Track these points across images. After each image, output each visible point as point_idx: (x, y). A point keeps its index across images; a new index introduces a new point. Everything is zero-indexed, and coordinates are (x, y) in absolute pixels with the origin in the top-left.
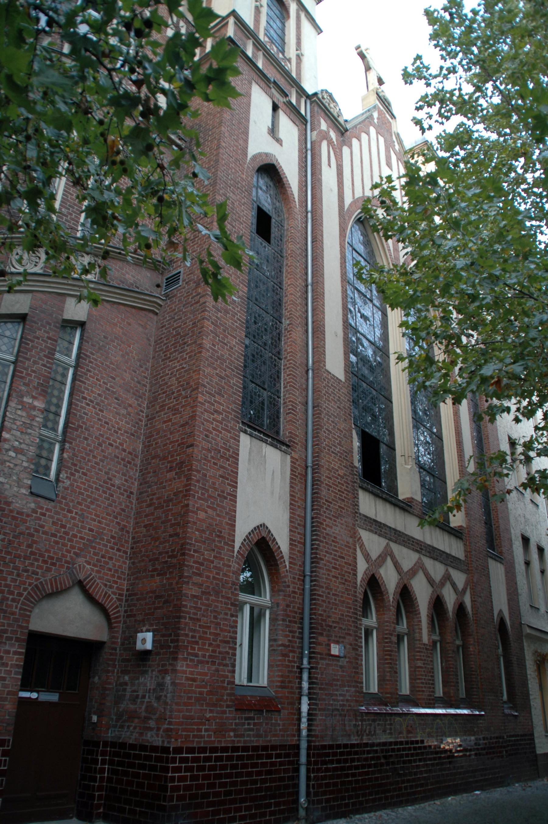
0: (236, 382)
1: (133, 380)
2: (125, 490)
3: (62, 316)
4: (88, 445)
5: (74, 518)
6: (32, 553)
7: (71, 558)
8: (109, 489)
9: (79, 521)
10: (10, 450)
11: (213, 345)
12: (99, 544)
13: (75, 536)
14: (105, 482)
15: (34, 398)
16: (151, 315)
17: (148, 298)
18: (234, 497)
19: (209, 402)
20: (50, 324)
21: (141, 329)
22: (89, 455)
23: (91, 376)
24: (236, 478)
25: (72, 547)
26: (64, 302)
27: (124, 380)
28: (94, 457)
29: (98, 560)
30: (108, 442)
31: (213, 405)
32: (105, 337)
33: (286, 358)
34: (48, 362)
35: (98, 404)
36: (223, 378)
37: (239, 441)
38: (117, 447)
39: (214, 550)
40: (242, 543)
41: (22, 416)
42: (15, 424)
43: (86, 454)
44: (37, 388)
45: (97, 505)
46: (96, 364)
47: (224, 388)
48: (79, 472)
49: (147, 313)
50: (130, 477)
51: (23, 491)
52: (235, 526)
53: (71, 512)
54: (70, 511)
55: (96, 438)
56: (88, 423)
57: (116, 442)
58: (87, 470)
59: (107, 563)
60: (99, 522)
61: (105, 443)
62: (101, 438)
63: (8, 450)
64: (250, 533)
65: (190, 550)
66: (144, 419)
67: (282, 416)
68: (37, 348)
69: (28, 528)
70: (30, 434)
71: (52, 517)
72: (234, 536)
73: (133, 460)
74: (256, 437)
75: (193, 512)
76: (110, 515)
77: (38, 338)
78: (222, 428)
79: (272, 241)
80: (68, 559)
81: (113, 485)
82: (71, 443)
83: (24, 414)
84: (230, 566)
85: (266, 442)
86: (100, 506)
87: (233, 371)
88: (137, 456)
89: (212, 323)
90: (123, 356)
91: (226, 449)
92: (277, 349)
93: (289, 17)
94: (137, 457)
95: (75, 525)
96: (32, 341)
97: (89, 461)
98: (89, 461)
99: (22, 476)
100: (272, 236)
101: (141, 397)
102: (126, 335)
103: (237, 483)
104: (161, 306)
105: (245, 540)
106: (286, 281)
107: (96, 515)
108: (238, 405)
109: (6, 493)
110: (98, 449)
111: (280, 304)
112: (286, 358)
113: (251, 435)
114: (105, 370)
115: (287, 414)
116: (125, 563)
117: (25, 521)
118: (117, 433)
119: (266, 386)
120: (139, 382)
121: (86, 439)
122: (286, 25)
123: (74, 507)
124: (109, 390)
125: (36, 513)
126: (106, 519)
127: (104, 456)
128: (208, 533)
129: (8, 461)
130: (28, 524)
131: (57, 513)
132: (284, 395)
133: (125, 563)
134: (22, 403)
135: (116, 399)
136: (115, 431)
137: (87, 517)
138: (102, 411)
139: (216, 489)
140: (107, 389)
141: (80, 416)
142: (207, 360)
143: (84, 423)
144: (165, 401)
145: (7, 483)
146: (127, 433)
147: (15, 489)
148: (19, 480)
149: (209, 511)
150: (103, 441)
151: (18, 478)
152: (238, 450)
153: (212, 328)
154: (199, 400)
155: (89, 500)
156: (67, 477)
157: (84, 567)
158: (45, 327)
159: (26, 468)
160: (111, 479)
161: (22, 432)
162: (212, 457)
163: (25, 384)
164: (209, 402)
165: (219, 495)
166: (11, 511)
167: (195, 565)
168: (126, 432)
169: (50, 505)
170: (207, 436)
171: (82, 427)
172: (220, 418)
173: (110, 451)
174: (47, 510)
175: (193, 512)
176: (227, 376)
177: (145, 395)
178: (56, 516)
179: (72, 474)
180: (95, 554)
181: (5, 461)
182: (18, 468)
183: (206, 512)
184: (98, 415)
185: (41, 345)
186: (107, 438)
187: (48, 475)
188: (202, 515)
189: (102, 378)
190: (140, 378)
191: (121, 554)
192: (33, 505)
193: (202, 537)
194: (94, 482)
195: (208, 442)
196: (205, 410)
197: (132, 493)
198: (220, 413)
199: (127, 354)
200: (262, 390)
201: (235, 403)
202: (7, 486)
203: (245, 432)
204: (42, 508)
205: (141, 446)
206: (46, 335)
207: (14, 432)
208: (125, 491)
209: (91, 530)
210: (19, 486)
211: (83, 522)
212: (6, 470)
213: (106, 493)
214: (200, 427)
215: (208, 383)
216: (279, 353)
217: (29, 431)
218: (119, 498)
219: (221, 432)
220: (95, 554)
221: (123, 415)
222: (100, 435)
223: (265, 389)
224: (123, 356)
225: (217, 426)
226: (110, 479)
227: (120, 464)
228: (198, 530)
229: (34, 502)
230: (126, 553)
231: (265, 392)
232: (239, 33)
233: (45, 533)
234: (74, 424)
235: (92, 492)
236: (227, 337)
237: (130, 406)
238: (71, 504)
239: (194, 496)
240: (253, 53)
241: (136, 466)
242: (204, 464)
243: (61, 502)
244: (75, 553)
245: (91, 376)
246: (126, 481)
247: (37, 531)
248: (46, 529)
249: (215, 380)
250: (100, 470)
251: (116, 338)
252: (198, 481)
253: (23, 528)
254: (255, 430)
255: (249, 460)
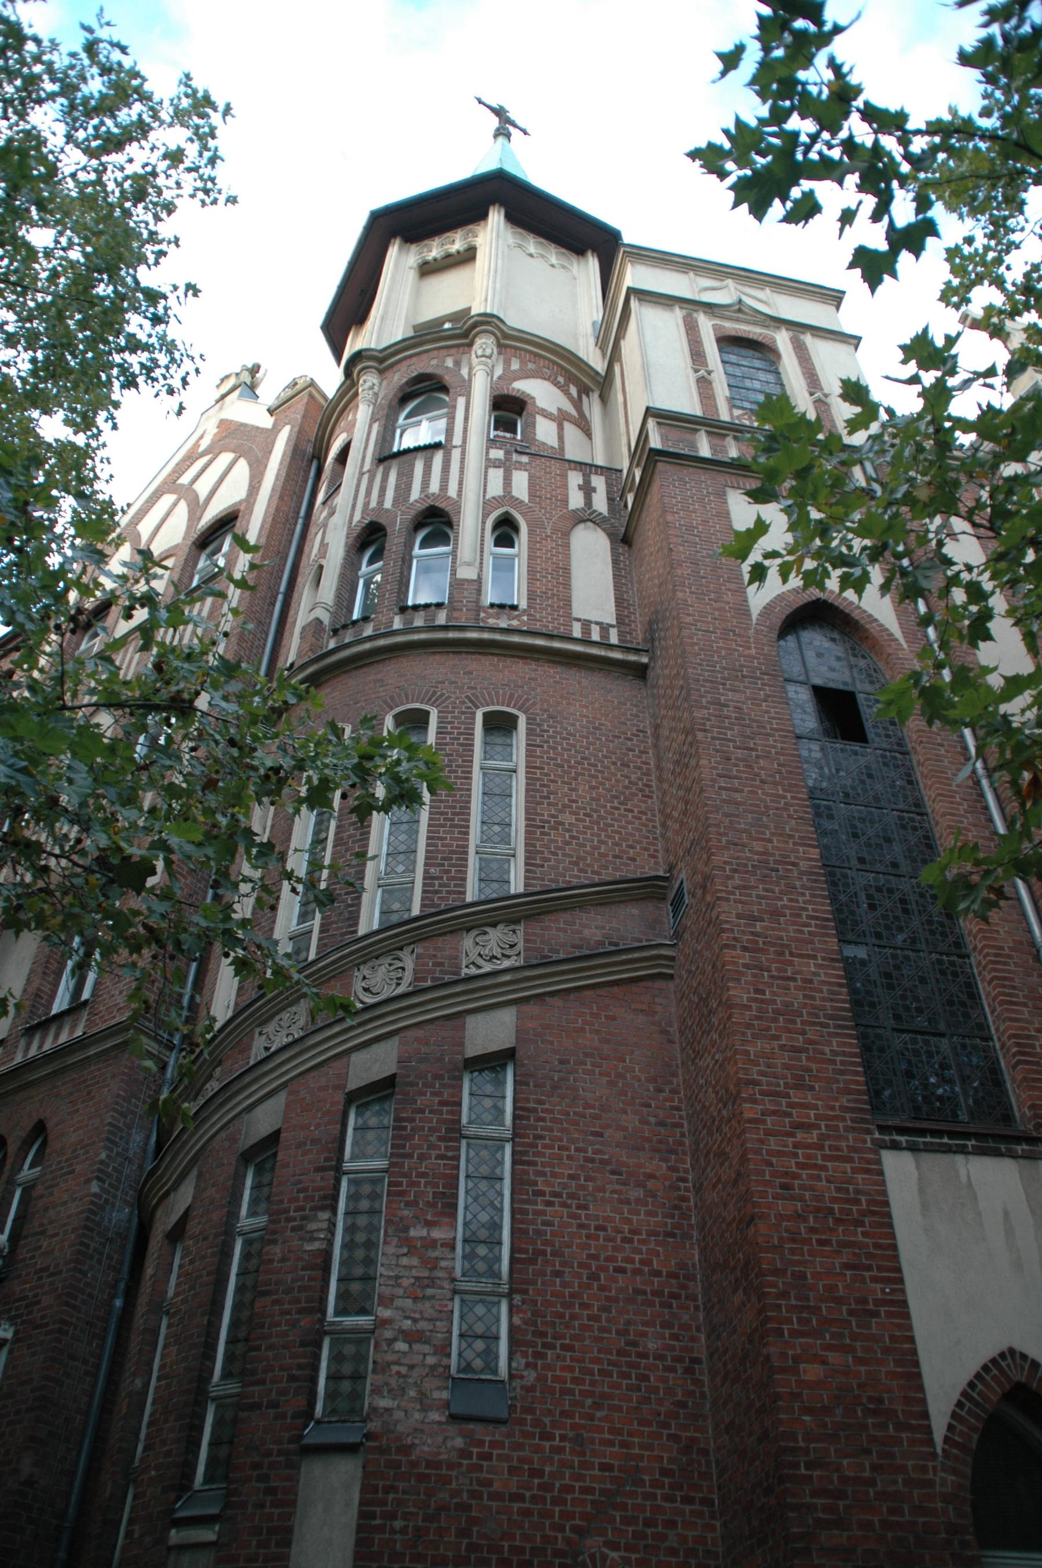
0: (841, 1046)
1: (648, 1123)
2: (676, 1359)
3: (462, 1053)
4: (565, 1285)
5: (560, 1450)
6: (472, 1548)
7: (568, 1541)
8: (636, 1366)
9: (573, 1451)
10: (395, 1339)
11: (757, 991)
12: (633, 1494)
13: (570, 1489)
14: (620, 1353)
15: (429, 1224)
16: (660, 984)
17: (636, 955)
18: (900, 1308)
19: (774, 1113)
20: (440, 1077)
21: (641, 1018)
22: (571, 1306)
23: (545, 1146)
24: (896, 1258)
25: (566, 1515)
26: (463, 1028)
27: (625, 1129)
28: (584, 1306)
29: (638, 1536)
30: (611, 1266)
31: (790, 1115)
32: (562, 1062)
33: (975, 949)
34: (447, 1148)
35: (571, 1196)
36: (800, 1050)
37: (881, 1173)
38: (636, 1272)
39: (868, 1452)
40: (954, 1415)
41: (411, 1267)
42: (399, 1285)
43: (564, 1305)
44: (432, 1205)
45: (611, 1408)
46: (552, 1120)
47: (808, 1070)
48: (552, 1347)
49: (649, 984)
50: (682, 1327)
51: (435, 1416)
52: (919, 1375)
53: (550, 1437)
54: (546, 1436)
55: (581, 1265)
56: (557, 1241)
57: (633, 1262)
58: (573, 1338)
59: (663, 1537)
60: (624, 1444)
61: (604, 1269)
62: (594, 1264)
63: (391, 1342)
64: (971, 1385)
65: (796, 1466)
66: (691, 1195)
67: (1007, 1077)
68: (422, 1128)
69: (455, 1493)
70: (433, 1297)
71: (508, 1458)
72: (923, 1401)
73: (684, 1287)
74: (929, 1149)
75: (783, 1370)
76: (649, 1424)
77: (422, 1111)
78: (825, 1158)
79: (871, 734)
80: (560, 1545)
81: (644, 1355)
82: (525, 1292)
83: (415, 1261)
84: (930, 1483)
85: (962, 1150)
86: (619, 1409)
87: (827, 1026)
88: (691, 1278)
89: (745, 949)
90: (611, 1084)
91: (848, 1201)
92: (951, 939)
93: (778, 356)
94: (693, 1279)
95: (563, 1464)
96: (412, 1120)
97: (573, 1317)
98: (573, 1317)
99: (429, 1384)
100: (868, 725)
101: (675, 1152)
102: (608, 1041)
103: (899, 1270)
104: (672, 959)
105: (959, 1404)
106: (928, 794)
107: (611, 1431)
108: (859, 1092)
109: (400, 1428)
110: (589, 1287)
111: (930, 846)
112: (975, 949)
113: (913, 1148)
114: (576, 1124)
115: (1014, 1068)
116: (713, 1528)
117: (448, 1480)
118: (630, 1241)
119: (942, 1027)
120: (662, 1124)
121: (558, 1274)
122: (781, 370)
123: (554, 1424)
124: (592, 1161)
125: (470, 1455)
126: (641, 1434)
127: (608, 1299)
128: (839, 1411)
129: (397, 1363)
130: (454, 1485)
131: (519, 1447)
132: (997, 1030)
133: (713, 1528)
134: (407, 1242)
135: (613, 1172)
136: (624, 1240)
137: (592, 1441)
138: (586, 1207)
139: (839, 1301)
140: (586, 1159)
141: (537, 1232)
142: (749, 1026)
143: (546, 1243)
144: (707, 1143)
145: (399, 1407)
146: (655, 1234)
147: (417, 1416)
148: (422, 1395)
149: (832, 1357)
150: (600, 1268)
151: (420, 1392)
152: (884, 1193)
153: (746, 958)
154: (747, 1115)
155: (589, 1401)
156: (528, 1365)
157: (604, 1557)
158: (432, 1086)
159: (433, 1368)
160: (635, 1344)
161: (416, 1299)
162: (813, 1230)
163: (408, 1204)
164: (774, 1113)
165: (851, 1312)
166: (414, 1464)
167: (820, 1501)
168: (650, 1233)
169: (498, 1434)
170: (785, 1187)
171: (544, 1253)
172: (814, 1136)
173: (621, 1284)
174: (493, 1444)
175: (783, 1370)
176: (812, 1042)
177: (681, 1144)
178: (515, 1455)
179: (538, 1355)
180: (626, 1521)
181: (389, 1364)
182: (416, 1373)
183: (824, 1362)
184: (576, 1217)
185: (431, 1121)
186: (608, 1259)
187: (495, 1372)
188: (812, 1372)
189: (572, 1141)
190: (661, 1113)
191: (696, 1507)
192: (459, 1442)
193: (824, 1425)
194: (593, 1361)
195: (793, 1198)
196: (768, 1133)
197: (696, 1361)
198: (807, 1127)
199: (620, 1076)
200: (933, 1040)
201: (847, 1091)
202: (399, 1415)
203: (895, 1146)
204: (481, 1443)
205: (696, 1253)
206: (437, 1099)
207: (398, 1302)
208: (678, 1359)
209: (605, 1467)
210: (425, 1409)
211: (583, 1454)
212: (393, 1382)
213: (628, 1376)
214: (762, 1173)
215: (763, 1074)
216: (958, 945)
217: (429, 1291)
218: (665, 1380)
219: (824, 1168)
220: (626, 1521)
221: (638, 1201)
222: (589, 1256)
223: (942, 1035)
224: (611, 1084)
225: (808, 1156)
226: (635, 1344)
227: (652, 1304)
228: (809, 1411)
229: (463, 1434)
230: (709, 1503)
231: (945, 1041)
232: (674, 434)
233: (495, 1496)
234: (526, 1251)
235: (593, 1383)
236: (791, 963)
237: (651, 1176)
238: (547, 1420)
239: (780, 1332)
240: (713, 447)
241: (695, 1299)
242: (792, 1252)
243: (522, 1422)
244: (575, 1529)
245: (545, 1146)
246: (675, 1337)
247: (475, 1495)
248: (497, 1486)
249: (779, 1062)
250: (603, 1330)
251: (586, 1055)
252: (784, 1295)
253: (443, 1495)
254: (922, 1132)
255: (925, 1206)
